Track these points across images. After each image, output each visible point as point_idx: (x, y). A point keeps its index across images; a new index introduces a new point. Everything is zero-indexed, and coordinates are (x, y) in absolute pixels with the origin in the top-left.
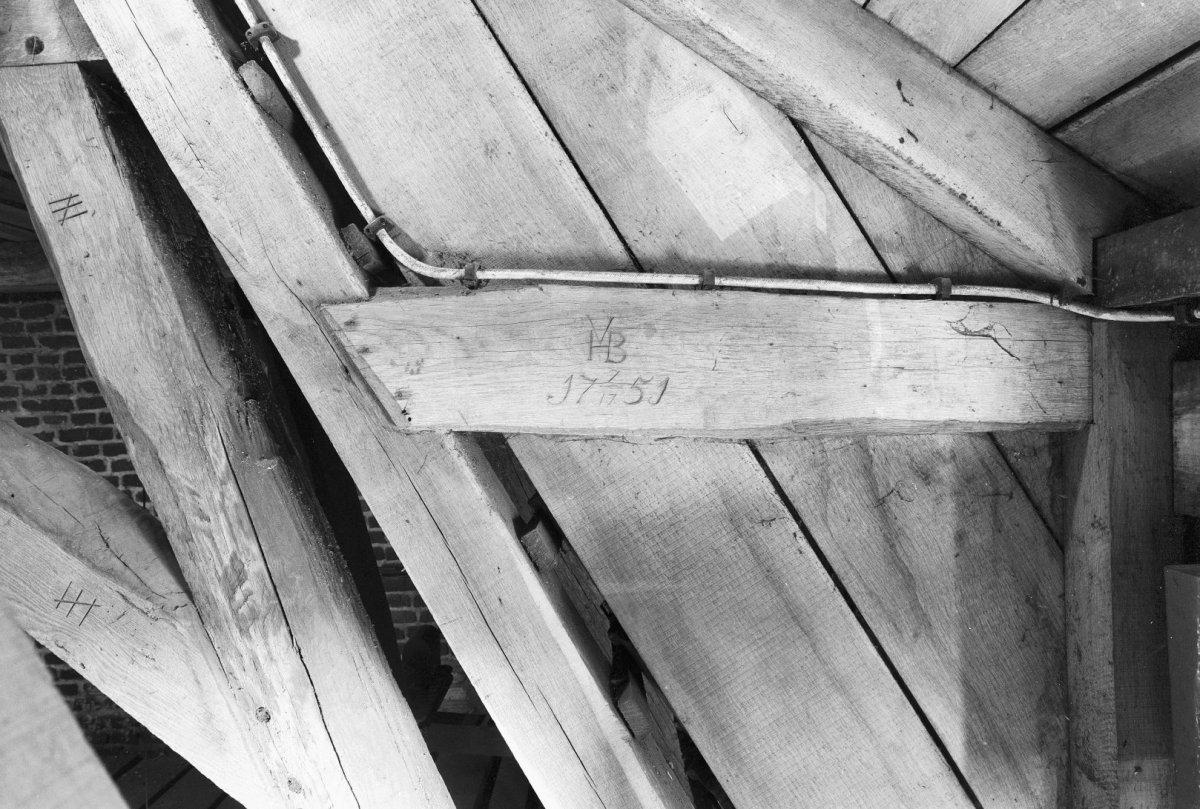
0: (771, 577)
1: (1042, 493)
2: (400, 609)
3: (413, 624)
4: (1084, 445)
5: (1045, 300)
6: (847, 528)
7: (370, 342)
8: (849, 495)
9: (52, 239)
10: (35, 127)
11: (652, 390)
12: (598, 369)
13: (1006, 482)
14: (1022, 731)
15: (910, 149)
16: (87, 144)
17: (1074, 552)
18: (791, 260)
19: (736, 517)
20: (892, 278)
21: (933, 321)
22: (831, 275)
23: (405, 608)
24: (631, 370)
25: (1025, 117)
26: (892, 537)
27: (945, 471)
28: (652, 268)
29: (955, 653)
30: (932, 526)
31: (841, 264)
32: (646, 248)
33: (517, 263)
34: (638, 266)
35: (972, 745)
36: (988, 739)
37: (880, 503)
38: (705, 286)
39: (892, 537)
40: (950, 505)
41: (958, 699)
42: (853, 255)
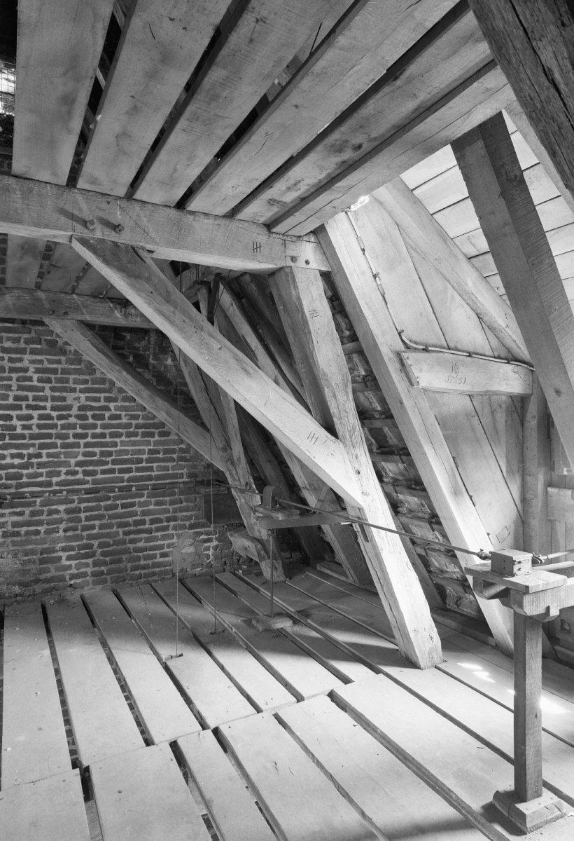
0: (473, 430)
1: (519, 411)
2: (161, 507)
3: (168, 515)
4: (530, 400)
5: (526, 366)
6: (487, 420)
7: (412, 363)
8: (487, 410)
9: (310, 323)
10: (306, 286)
11: (463, 380)
12: (454, 375)
13: (514, 409)
14: (515, 468)
15: (507, 329)
16: (320, 295)
17: (526, 424)
18: (478, 351)
19: (468, 416)
20: (495, 358)
21: (508, 369)
22: (485, 356)
23: (164, 507)
24: (460, 375)
25: (464, 254)
26: (494, 421)
27: (504, 406)
28: (452, 350)
29: (505, 450)
30: (501, 417)
31: (487, 353)
32: (451, 345)
33: (436, 346)
34: (449, 349)
35: (507, 472)
36: (510, 471)
37: (492, 413)
38: (470, 356)
39: (494, 421)
40: (504, 414)
41: (505, 460)
42: (489, 352)
